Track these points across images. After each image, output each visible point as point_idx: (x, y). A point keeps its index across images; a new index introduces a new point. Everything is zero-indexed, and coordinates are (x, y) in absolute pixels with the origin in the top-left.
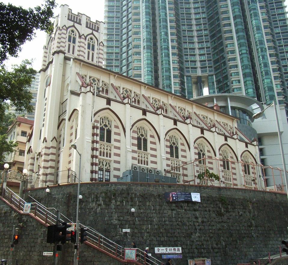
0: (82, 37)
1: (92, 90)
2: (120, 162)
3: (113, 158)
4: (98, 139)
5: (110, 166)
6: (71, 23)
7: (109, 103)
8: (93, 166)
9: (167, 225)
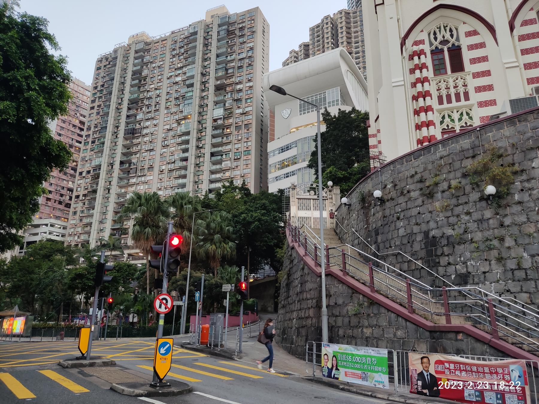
2: (495, 100)
3: (475, 98)
4: (429, 73)
5: (471, 118)
8: (430, 128)
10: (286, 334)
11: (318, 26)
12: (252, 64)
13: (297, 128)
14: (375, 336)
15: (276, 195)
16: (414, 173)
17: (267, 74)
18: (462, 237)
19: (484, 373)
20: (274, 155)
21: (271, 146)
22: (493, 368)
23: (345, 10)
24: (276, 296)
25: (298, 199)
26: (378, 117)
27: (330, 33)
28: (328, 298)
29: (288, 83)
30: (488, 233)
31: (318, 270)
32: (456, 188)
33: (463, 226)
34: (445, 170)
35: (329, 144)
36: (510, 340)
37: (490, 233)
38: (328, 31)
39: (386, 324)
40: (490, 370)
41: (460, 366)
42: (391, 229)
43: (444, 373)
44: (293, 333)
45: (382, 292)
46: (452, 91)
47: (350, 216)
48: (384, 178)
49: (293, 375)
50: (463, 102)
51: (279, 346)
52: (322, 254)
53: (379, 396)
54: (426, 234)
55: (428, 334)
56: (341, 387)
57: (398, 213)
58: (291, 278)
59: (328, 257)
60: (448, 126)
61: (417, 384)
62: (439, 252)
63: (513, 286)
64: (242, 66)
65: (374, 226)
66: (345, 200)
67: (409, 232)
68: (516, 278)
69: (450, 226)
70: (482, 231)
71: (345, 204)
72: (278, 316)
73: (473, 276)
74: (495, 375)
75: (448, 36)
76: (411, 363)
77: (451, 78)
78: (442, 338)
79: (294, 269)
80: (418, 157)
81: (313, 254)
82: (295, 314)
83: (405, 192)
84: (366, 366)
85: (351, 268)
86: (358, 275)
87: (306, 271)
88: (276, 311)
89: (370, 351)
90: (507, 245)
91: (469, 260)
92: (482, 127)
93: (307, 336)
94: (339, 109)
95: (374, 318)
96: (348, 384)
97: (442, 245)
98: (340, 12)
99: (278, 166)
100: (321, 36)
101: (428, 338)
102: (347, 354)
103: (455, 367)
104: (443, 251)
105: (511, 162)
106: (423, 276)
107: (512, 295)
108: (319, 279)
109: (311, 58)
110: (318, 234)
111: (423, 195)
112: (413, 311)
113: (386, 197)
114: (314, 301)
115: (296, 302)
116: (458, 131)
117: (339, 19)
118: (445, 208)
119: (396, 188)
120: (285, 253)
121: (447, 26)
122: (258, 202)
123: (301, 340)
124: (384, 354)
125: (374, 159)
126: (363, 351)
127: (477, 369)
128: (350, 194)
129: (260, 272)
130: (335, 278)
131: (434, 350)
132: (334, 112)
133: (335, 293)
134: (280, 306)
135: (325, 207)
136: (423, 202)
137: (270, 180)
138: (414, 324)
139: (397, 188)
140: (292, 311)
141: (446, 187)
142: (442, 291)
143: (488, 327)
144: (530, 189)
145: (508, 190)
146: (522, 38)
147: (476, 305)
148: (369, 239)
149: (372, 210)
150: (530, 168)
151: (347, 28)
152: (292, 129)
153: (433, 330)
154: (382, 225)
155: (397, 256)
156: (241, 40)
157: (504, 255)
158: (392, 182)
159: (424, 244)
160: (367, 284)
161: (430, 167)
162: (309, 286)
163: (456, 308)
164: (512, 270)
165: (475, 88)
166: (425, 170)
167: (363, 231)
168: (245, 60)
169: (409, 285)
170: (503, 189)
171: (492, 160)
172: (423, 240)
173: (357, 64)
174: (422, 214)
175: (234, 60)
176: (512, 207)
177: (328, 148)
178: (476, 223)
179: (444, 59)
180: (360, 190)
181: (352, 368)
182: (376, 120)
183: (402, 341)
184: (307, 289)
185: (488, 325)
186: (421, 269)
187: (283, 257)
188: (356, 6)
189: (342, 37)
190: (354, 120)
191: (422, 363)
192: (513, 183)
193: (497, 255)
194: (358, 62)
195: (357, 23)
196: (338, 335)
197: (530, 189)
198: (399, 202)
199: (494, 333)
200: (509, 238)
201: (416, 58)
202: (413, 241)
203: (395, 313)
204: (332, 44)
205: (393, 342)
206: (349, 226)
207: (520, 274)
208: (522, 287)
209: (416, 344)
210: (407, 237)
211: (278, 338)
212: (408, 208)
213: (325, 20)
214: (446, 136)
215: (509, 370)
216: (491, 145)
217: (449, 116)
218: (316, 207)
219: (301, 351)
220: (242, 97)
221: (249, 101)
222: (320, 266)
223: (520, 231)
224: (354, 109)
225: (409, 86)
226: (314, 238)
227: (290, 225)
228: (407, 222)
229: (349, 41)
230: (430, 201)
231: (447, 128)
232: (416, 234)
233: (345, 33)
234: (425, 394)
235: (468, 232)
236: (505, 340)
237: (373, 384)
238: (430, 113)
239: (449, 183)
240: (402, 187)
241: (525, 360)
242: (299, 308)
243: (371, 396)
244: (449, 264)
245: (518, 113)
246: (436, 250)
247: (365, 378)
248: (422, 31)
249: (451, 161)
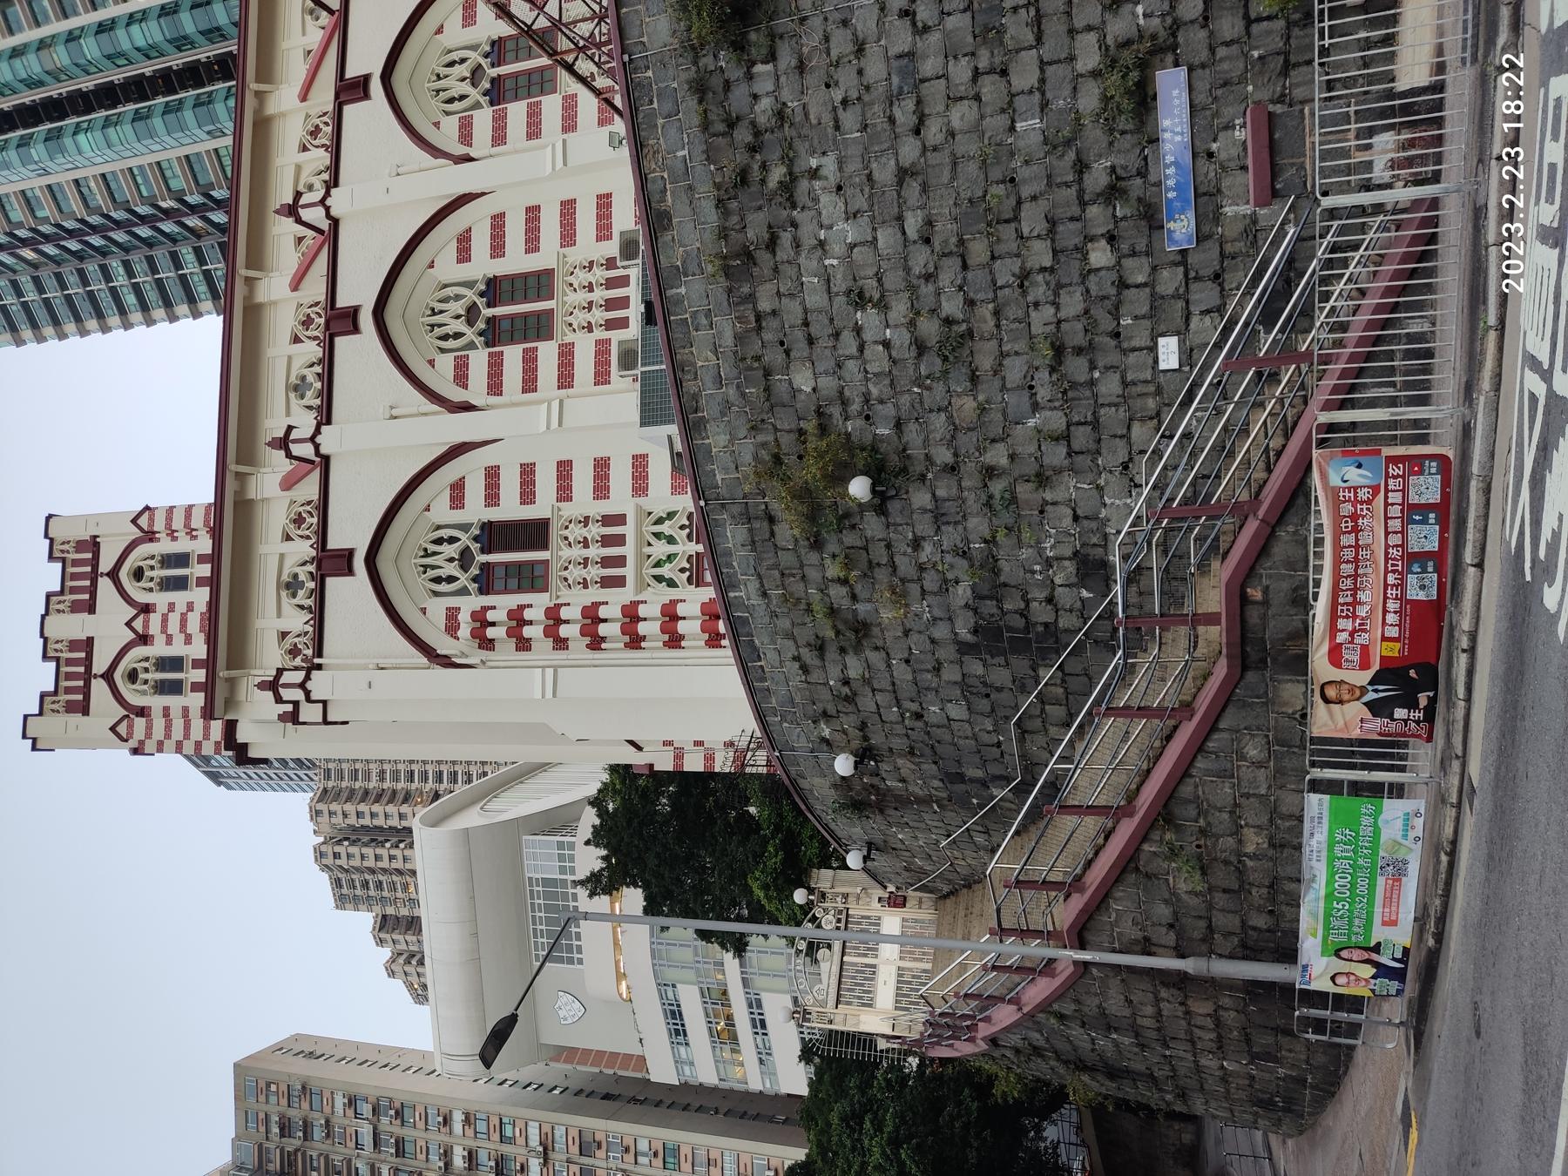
0: (140, 630)
1: (298, 677)
4: (537, 605)
5: (671, 515)
6: (99, 688)
7: (340, 562)
8: (680, 613)
9: (929, 223)
10: (1271, 1099)
11: (337, 883)
12: (397, 1105)
13: (620, 976)
14: (1264, 820)
15: (819, 1072)
16: (797, 665)
17: (437, 1057)
18: (977, 564)
19: (1357, 547)
20: (692, 1064)
21: (663, 1071)
22: (1343, 525)
23: (312, 799)
24: (1146, 1112)
25: (838, 1002)
26: (632, 743)
27: (365, 850)
28: (1154, 949)
29: (478, 996)
30: (970, 502)
31: (1064, 971)
32: (848, 564)
33: (948, 558)
34: (797, 588)
35: (681, 883)
36: (1260, 475)
37: (973, 501)
38: (359, 856)
39: (1227, 785)
40: (1349, 533)
41: (1343, 605)
42: (948, 737)
43: (1365, 649)
44: (1267, 1076)
45: (1134, 786)
46: (595, 552)
47: (903, 847)
48: (802, 743)
49: (1406, 1096)
50: (629, 530)
51: (1313, 1126)
52: (1015, 951)
53: (1448, 830)
54: (964, 649)
55: (1251, 676)
56: (1431, 942)
57: (902, 715)
58: (1090, 1058)
59: (1025, 934)
60: (682, 570)
61: (1405, 721)
62: (1019, 622)
63: (1114, 455)
64: (397, 1142)
65: (936, 783)
66: (854, 859)
67: (959, 692)
68: (1092, 446)
69: (947, 590)
70: (964, 516)
71: (866, 859)
72: (1214, 1117)
73: (1083, 545)
74: (1360, 521)
75: (451, 550)
76: (1341, 730)
77: (560, 553)
78: (1263, 640)
79: (1062, 1046)
80: (755, 649)
81: (1016, 978)
82: (1208, 1062)
83: (846, 690)
84: (1361, 862)
85: (1060, 867)
86: (1082, 846)
87: (1068, 1008)
88: (1192, 1119)
89: (1314, 842)
90: (1004, 461)
91: (1041, 551)
92: (699, 493)
93: (1277, 1030)
94: (587, 843)
95: (1210, 819)
96: (1420, 920)
97: (999, 612)
98: (316, 814)
99: (727, 1055)
100: (367, 877)
101: (1263, 675)
102: (1328, 915)
103: (1347, 617)
104: (1016, 612)
105: (794, 436)
106: (1085, 669)
107: (1136, 458)
108: (1094, 971)
109: (423, 912)
110: (951, 953)
111: (858, 648)
112: (1187, 708)
113: (856, 744)
114: (1164, 993)
115: (1168, 1053)
116: (700, 548)
117: (334, 820)
118: (899, 596)
119: (834, 713)
120: (1009, 1068)
121: (426, 550)
122: (835, 1139)
123: (1290, 1051)
124: (1320, 804)
125: (743, 765)
126: (1314, 863)
127: (1348, 562)
128: (838, 840)
129: (1064, 1158)
130: (1090, 918)
131: (1299, 665)
132: (590, 860)
133: (1137, 924)
134: (1179, 1107)
135: (869, 918)
136: (877, 648)
137: (768, 1085)
138: (1223, 710)
139: (831, 710)
140: (1198, 1069)
141: (844, 590)
142: (1126, 629)
143: (1226, 523)
144: (867, 401)
145: (863, 449)
146: (495, 387)
147: (1164, 547)
148: (975, 801)
149: (889, 783)
150: (814, 397)
151: (363, 800)
152: (621, 995)
153: (1239, 662)
154: (935, 763)
155: (1026, 732)
156: (318, 1134)
157: (1030, 468)
158: (814, 722)
159: (992, 657)
160: (1110, 825)
161: (784, 623)
162: (1115, 1004)
163: (1172, 596)
164: (1070, 454)
165: (596, 498)
166: (790, 636)
167: (950, 816)
168: (381, 1128)
169: (1111, 711)
170: (861, 459)
171: (785, 479)
172: (981, 659)
173: (470, 781)
174: (911, 653)
175: (372, 1167)
176: (907, 443)
177: (693, 887)
178: (943, 528)
179: (507, 565)
180: (830, 811)
181: (1371, 903)
182: (639, 748)
183: (1276, 748)
184: (1127, 1012)
185: (1219, 523)
186: (1063, 671)
187: (1020, 1078)
188: (309, 768)
189: (386, 815)
190: (626, 806)
191: (1341, 702)
192: (848, 435)
193: (1030, 486)
194: (465, 778)
195: (356, 771)
196: (1268, 931)
197: (867, 401)
198: (874, 708)
199: (1242, 512)
200: (988, 455)
201: (491, 632)
202: (985, 684)
203: (1195, 757)
204: (397, 847)
205: (1280, 772)
206: (931, 853)
207: (1082, 437)
208: (1115, 436)
209: (1284, 710)
210: (972, 698)
211: (1284, 1127)
212: (890, 688)
213: (325, 861)
214: (708, 577)
215: (1344, 489)
216: (746, 478)
217: (658, 564)
218: (869, 949)
219: (1325, 1053)
220: (493, 1153)
221: (508, 1132)
222: (1051, 961)
223: (970, 429)
224: (596, 802)
225: (561, 655)
226: (963, 967)
227: (918, 1043)
228: (931, 696)
229: (401, 797)
230: (876, 631)
231: (688, 573)
232: (963, 675)
233: (377, 808)
234: (1433, 701)
235: (966, 549)
236: (1261, 488)
237: (1413, 846)
238: (642, 611)
239: (832, 581)
240: (830, 698)
241: (1314, 451)
242: (1188, 1047)
243: (1453, 854)
244: (1050, 600)
245: (675, 411)
246: (1010, 629)
247: (1398, 870)
248: (424, 611)
249: (776, 573)
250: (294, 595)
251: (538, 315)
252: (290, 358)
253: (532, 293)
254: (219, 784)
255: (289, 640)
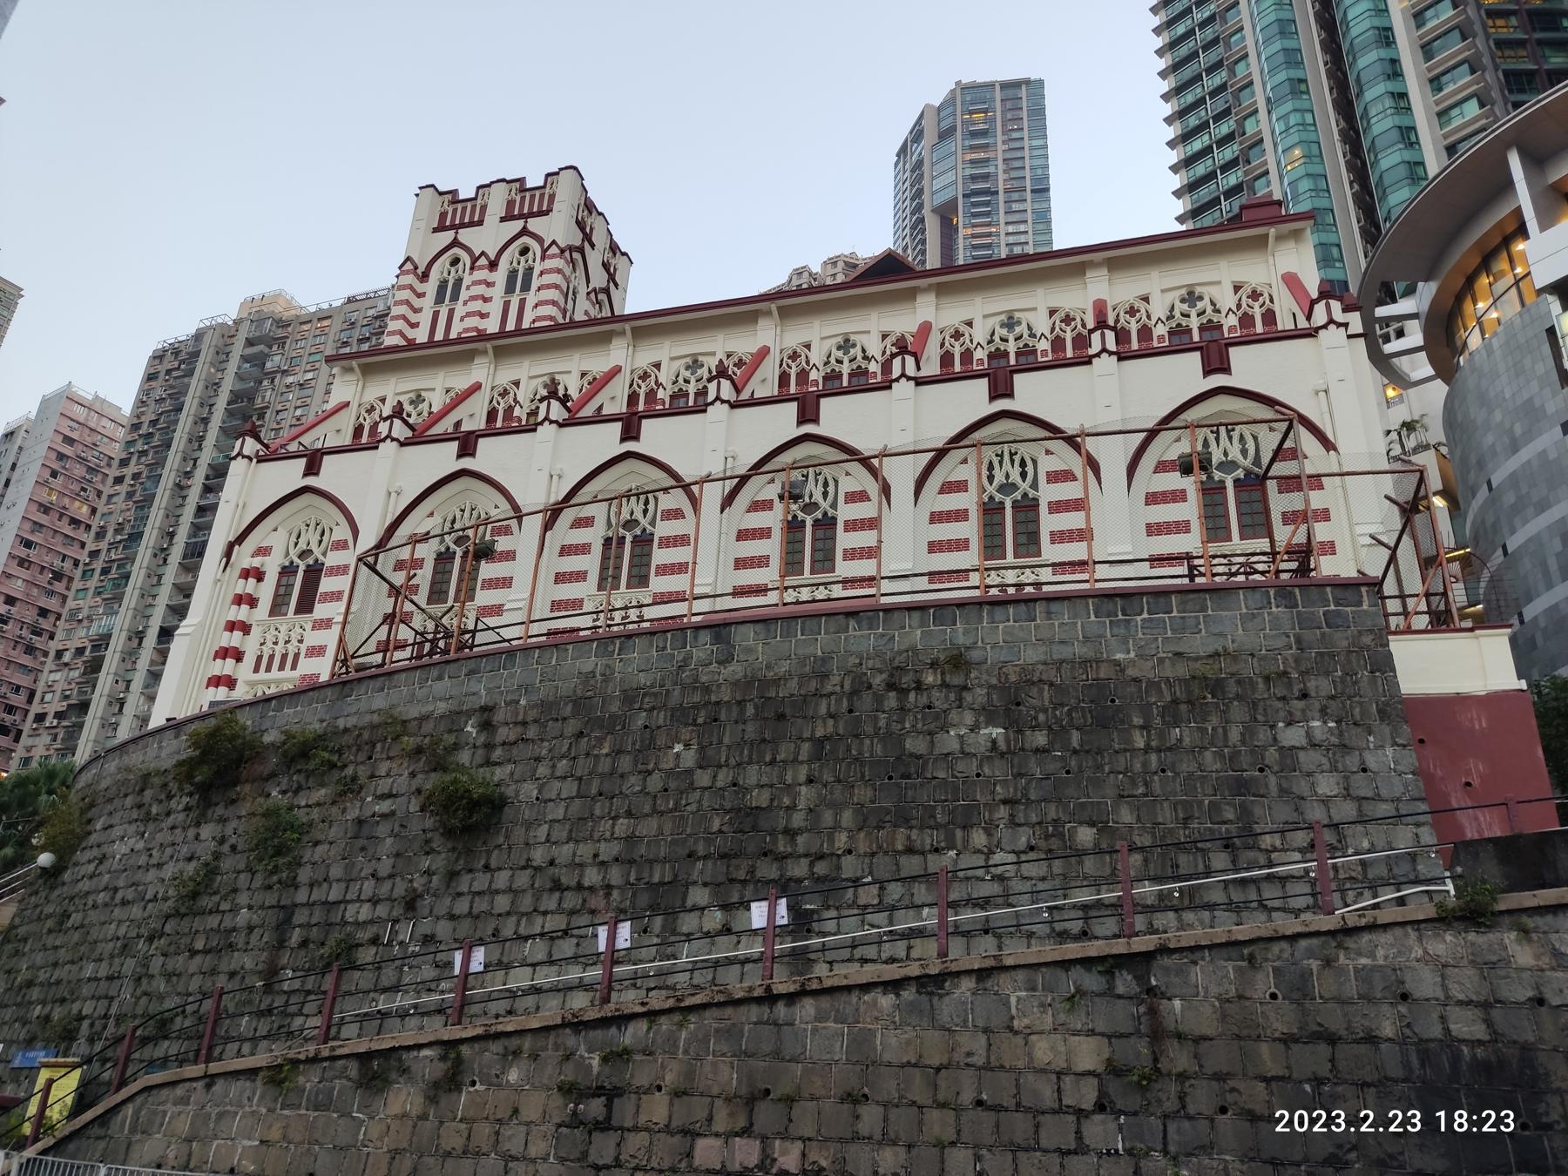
46: (279, 650)
75: (1015, 476)
250: (1183, 301)
251: (1228, 528)
252: (1035, 309)
253: (1247, 520)
254: (898, 155)
255: (1142, 306)
